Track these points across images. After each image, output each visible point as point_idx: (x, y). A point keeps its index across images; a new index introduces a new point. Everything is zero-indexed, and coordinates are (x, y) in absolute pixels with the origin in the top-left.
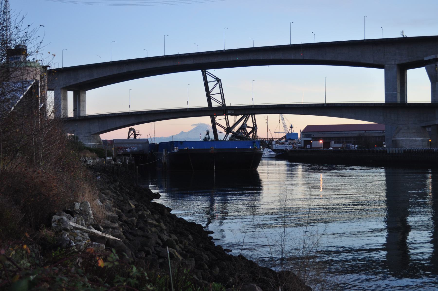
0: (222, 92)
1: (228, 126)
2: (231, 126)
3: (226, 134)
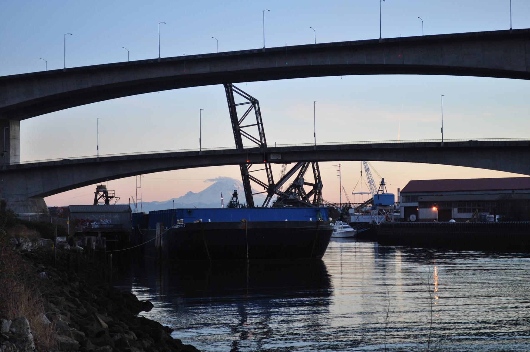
0: (260, 122)
1: (271, 183)
2: (276, 181)
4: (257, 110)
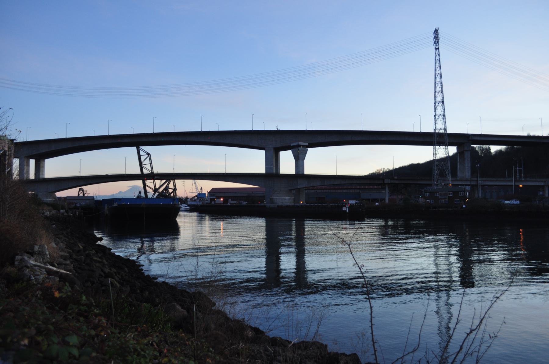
0: (151, 163)
3: (154, 193)
4: (150, 158)
